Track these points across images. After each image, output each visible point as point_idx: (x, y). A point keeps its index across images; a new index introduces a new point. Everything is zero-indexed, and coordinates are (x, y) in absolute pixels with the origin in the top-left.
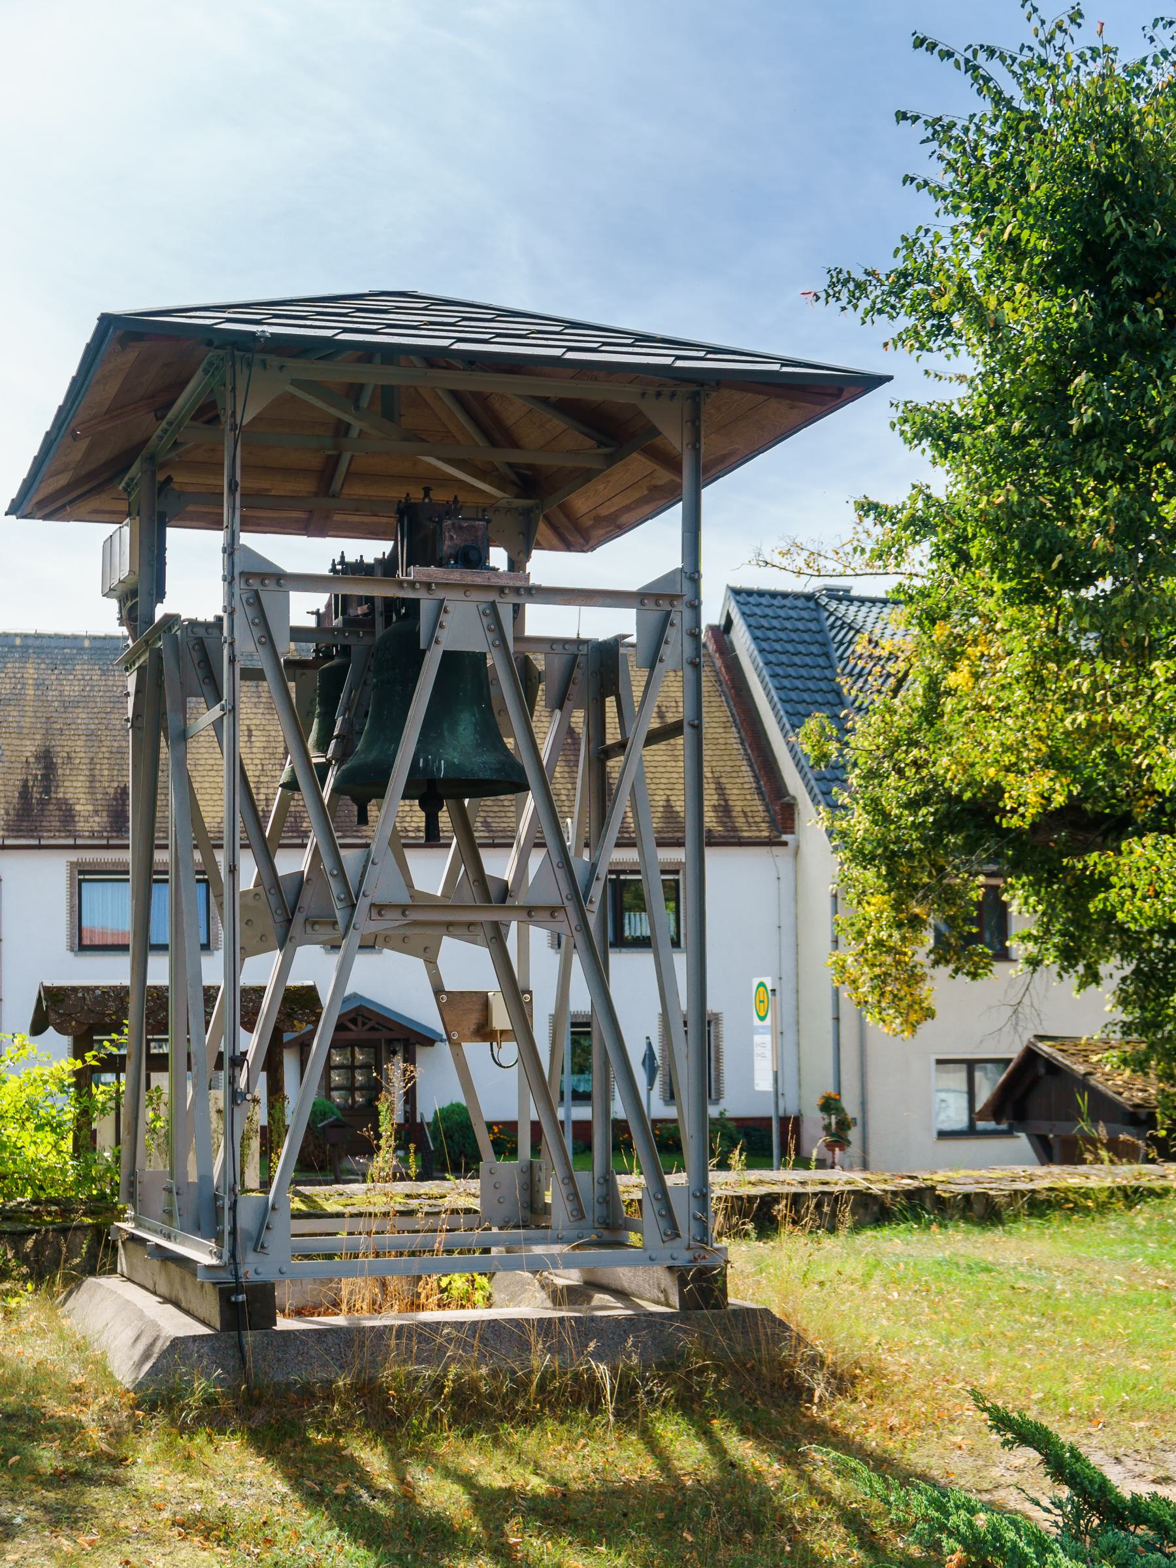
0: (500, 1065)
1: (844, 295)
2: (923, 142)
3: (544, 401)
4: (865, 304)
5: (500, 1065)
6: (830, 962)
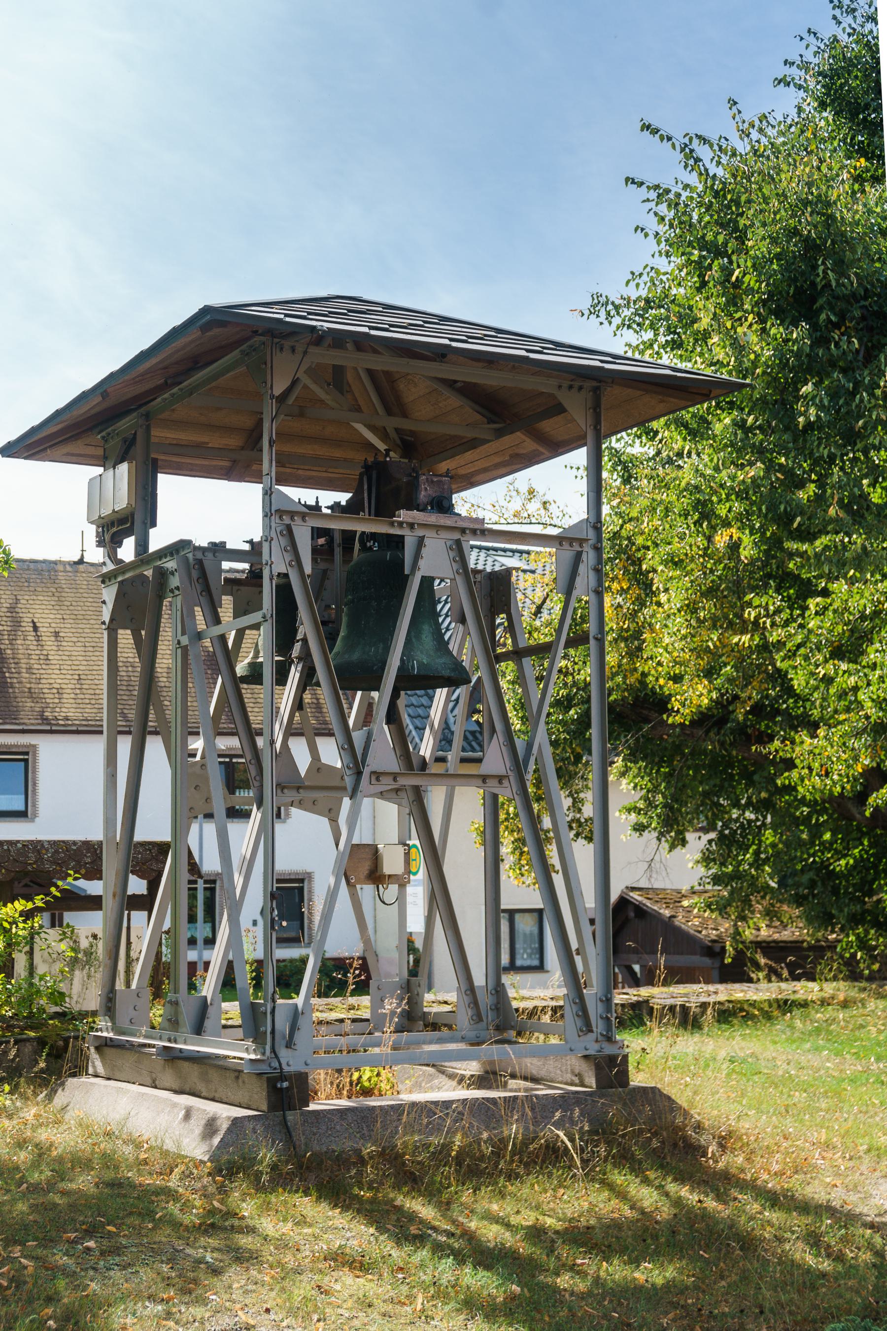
0: (384, 902)
1: (603, 314)
2: (644, 201)
3: (451, 384)
4: (617, 321)
5: (384, 902)
6: (473, 828)
